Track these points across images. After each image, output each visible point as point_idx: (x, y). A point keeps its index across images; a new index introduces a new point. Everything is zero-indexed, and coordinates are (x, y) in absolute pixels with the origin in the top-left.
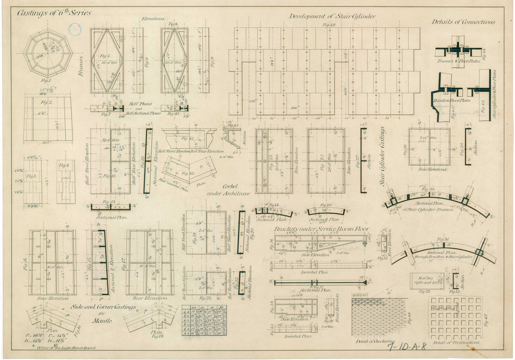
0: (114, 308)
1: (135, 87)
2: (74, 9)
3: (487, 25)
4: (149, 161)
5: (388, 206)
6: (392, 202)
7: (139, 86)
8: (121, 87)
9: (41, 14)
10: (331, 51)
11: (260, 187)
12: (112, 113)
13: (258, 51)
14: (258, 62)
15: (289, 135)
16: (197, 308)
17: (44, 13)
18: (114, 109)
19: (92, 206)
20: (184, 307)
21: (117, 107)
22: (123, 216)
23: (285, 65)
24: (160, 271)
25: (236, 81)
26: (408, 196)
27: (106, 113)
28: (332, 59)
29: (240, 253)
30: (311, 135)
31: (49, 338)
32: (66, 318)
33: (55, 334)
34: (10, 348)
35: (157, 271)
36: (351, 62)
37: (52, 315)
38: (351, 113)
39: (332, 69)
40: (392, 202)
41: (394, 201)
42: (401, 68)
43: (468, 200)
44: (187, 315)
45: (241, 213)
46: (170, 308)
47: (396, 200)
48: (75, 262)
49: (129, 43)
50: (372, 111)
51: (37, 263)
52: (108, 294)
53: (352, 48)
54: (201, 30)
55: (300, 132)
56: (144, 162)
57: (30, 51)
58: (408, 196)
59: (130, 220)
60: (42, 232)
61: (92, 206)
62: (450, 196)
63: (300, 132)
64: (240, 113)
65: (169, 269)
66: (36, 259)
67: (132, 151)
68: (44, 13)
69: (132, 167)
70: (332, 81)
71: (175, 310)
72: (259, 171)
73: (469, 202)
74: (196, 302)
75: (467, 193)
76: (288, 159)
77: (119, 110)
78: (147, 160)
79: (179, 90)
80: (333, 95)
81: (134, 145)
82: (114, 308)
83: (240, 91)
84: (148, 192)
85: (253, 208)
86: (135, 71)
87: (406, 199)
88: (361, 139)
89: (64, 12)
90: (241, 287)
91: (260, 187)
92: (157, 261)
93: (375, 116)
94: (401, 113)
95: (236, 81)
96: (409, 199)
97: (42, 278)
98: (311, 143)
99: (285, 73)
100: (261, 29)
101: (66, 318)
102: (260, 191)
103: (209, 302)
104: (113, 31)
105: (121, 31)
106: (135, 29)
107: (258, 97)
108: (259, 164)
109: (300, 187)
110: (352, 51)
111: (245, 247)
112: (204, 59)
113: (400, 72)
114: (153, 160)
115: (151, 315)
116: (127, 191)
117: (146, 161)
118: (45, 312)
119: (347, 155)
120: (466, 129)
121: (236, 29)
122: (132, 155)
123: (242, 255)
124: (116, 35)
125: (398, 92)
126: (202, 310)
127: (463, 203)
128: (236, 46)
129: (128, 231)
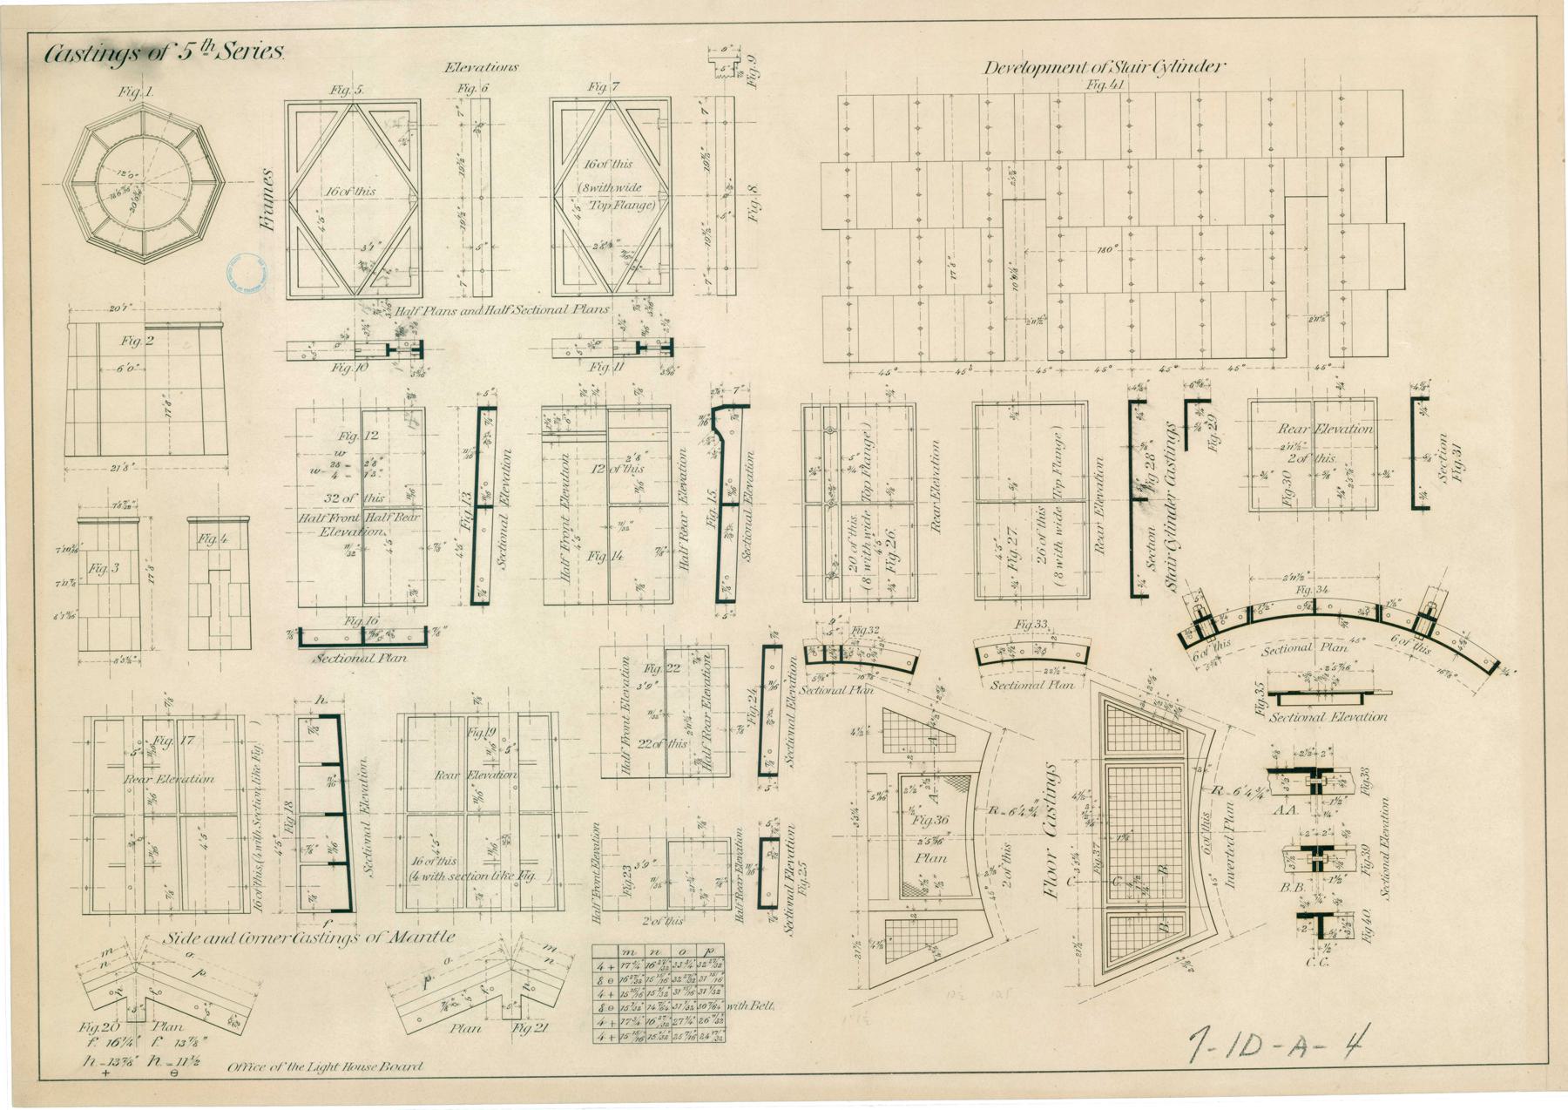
1: (467, 278)
2: (233, 36)
4: (486, 507)
6: (1198, 630)
7: (722, 273)
8: (666, 277)
10: (992, 165)
11: (815, 583)
12: (631, 363)
13: (1052, 166)
14: (1335, 197)
16: (640, 952)
20: (598, 952)
21: (651, 342)
23: (852, 209)
24: (515, 840)
25: (986, 257)
26: (1250, 610)
28: (1278, 186)
30: (982, 424)
32: (193, 981)
33: (171, 1037)
34: (34, 1076)
35: (506, 840)
37: (158, 976)
38: (1337, 352)
39: (1279, 219)
40: (1198, 630)
41: (1207, 628)
42: (852, 217)
43: (1434, 620)
44: (606, 977)
46: (551, 956)
47: (1213, 623)
49: (690, 139)
52: (350, 911)
54: (708, 106)
56: (472, 510)
57: (86, 172)
65: (549, 832)
66: (110, 800)
67: (677, 473)
69: (677, 522)
71: (568, 961)
72: (814, 536)
74: (627, 931)
75: (1430, 598)
78: (480, 502)
79: (374, 291)
83: (1280, 286)
89: (195, 49)
91: (815, 583)
92: (505, 809)
93: (1269, 363)
95: (986, 257)
97: (130, 861)
100: (1132, 97)
101: (193, 981)
102: (818, 595)
103: (674, 934)
106: (711, 100)
107: (1055, 308)
108: (814, 514)
113: (851, 233)
114: (497, 503)
115: (481, 978)
116: (663, 594)
117: (722, 505)
118: (140, 969)
119: (1094, 482)
120: (1187, 402)
121: (842, 100)
122: (677, 487)
126: (661, 963)
127: (1418, 629)
128: (984, 150)
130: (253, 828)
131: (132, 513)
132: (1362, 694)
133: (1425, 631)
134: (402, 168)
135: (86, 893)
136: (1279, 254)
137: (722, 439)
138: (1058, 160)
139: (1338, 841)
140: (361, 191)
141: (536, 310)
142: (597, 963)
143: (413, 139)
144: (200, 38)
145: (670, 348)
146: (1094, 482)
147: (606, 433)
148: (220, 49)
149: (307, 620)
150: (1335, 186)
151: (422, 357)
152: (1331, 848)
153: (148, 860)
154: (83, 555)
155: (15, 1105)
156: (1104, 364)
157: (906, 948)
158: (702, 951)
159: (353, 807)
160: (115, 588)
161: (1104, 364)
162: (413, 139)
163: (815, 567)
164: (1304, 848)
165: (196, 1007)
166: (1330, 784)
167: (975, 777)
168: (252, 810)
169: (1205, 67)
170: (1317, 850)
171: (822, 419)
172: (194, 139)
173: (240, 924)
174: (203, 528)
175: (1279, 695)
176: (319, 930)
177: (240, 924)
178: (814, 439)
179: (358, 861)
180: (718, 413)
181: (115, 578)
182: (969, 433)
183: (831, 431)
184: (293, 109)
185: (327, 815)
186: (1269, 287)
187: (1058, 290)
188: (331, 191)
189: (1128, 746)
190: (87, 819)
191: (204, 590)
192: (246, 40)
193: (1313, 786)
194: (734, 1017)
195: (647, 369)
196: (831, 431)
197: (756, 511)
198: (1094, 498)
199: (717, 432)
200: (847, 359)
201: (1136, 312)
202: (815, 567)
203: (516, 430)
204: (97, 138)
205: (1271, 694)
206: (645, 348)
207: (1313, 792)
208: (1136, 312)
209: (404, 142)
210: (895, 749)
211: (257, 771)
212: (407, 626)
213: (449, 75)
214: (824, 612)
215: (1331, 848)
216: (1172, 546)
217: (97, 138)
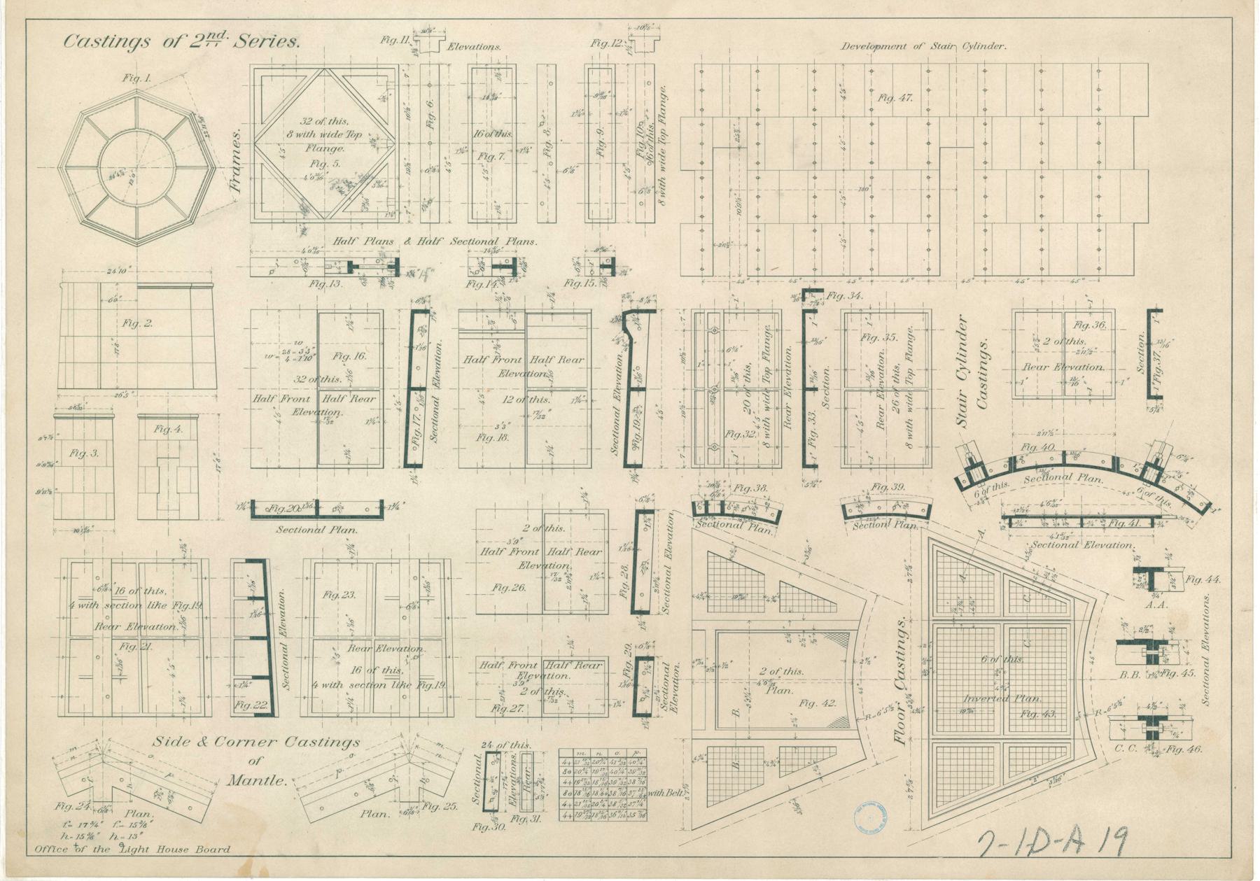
3: (894, 51)
9: (134, 44)
17: (142, 42)
18: (351, 267)
19: (253, 507)
27: (321, 280)
29: (642, 613)
31: (64, 830)
36: (753, 149)
39: (935, 165)
43: (981, 464)
45: (258, 512)
47: (1159, 476)
61: (253, 507)
62: (1116, 461)
64: (934, 271)
70: (708, 195)
73: (988, 468)
80: (935, 228)
86: (444, 173)
96: (1016, 470)
99: (875, 174)
100: (817, 67)
110: (756, 121)
121: (698, 68)
123: (644, 617)
132: (1152, 518)
135: (208, 692)
136: (934, 195)
137: (631, 338)
139: (1173, 711)
147: (525, 331)
152: (1165, 718)
153: (116, 673)
155: (7, 876)
157: (742, 787)
159: (275, 632)
162: (391, 99)
164: (1141, 718)
165: (356, 794)
166: (1170, 654)
167: (853, 634)
169: (993, 46)
170: (1153, 720)
179: (279, 677)
180: (628, 317)
183: (715, 331)
184: (259, 73)
185: (253, 638)
186: (925, 219)
189: (1046, 609)
193: (1149, 657)
200: (700, 273)
204: (136, 105)
206: (357, 267)
210: (717, 609)
214: (709, 476)
215: (1165, 718)
217: (136, 105)
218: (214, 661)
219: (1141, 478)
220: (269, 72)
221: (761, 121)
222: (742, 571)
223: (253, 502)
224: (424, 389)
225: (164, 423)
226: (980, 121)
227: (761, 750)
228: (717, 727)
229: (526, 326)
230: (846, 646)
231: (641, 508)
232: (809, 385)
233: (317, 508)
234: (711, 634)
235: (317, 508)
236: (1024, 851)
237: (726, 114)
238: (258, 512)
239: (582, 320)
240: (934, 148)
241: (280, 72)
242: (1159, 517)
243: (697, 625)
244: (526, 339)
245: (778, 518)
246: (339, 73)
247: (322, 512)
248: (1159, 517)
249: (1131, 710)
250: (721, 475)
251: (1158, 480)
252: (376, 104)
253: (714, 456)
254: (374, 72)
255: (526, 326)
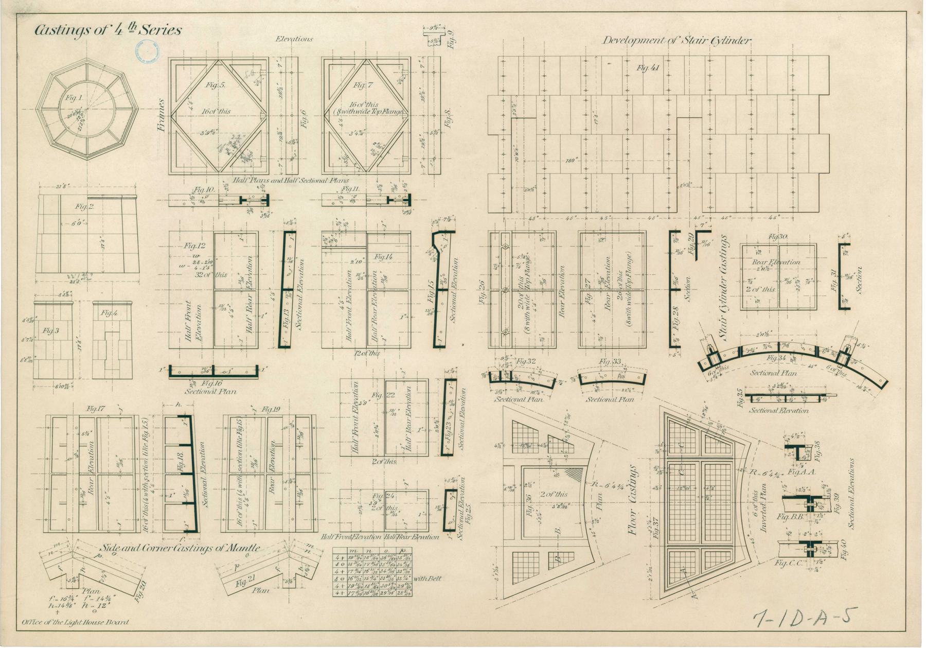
0: (172, 549)
4: (443, 290)
5: (704, 367)
11: (496, 336)
14: (540, 119)
15: (548, 242)
17: (85, 31)
18: (389, 200)
22: (628, 395)
26: (740, 349)
28: (673, 112)
39: (673, 131)
40: (839, 355)
43: (717, 352)
45: (173, 373)
47: (848, 360)
48: (315, 471)
50: (744, 206)
51: (61, 474)
53: (708, 92)
54: (282, 63)
55: (567, 240)
58: (740, 349)
59: (244, 396)
60: (286, 418)
62: (817, 349)
63: (567, 240)
64: (673, 209)
66: (59, 466)
68: (85, 31)
73: (721, 355)
75: (705, 344)
76: (547, 286)
77: (400, 203)
81: (302, 264)
82: (172, 549)
83: (673, 170)
84: (288, 345)
85: (486, 371)
87: (736, 355)
88: (670, 253)
90: (449, 513)
91: (496, 336)
94: (795, 210)
96: (743, 356)
97: (286, 502)
98: (584, 258)
104: (380, 62)
105: (405, 62)
106: (284, 59)
107: (541, 182)
109: (567, 339)
111: (457, 441)
112: (289, 113)
124: (389, 71)
125: (625, 171)
129: (226, 417)
130: (143, 482)
131: (69, 298)
132: (819, 395)
133: (718, 361)
134: (257, 100)
138: (544, 95)
140: (221, 111)
141: (312, 181)
142: (335, 556)
143: (264, 82)
144: (127, 20)
145: (409, 200)
146: (559, 279)
147: (366, 247)
148: (140, 28)
149: (173, 358)
150: (540, 113)
151: (268, 205)
154: (36, 322)
156: (653, 214)
158: (399, 550)
160: (57, 344)
161: (653, 214)
162: (264, 82)
163: (496, 328)
164: (801, 542)
168: (143, 471)
170: (810, 544)
171: (500, 243)
172: (119, 82)
173: (135, 540)
174: (102, 308)
175: (751, 395)
176: (176, 542)
177: (135, 540)
178: (496, 252)
181: (57, 336)
182: (576, 250)
183: (506, 247)
187: (709, 171)
188: (205, 111)
190: (225, 476)
191: (103, 343)
192: (157, 21)
194: (418, 587)
195: (395, 214)
196: (506, 247)
197: (458, 293)
198: (559, 288)
199: (435, 247)
200: (584, 210)
201: (795, 184)
202: (496, 328)
203: (306, 248)
204: (58, 81)
205: (747, 395)
206: (245, 200)
207: (808, 511)
208: (795, 184)
209: (258, 83)
211: (145, 448)
212: (241, 363)
213: (278, 43)
214: (501, 353)
216: (723, 309)
217: (58, 81)
218: (41, 486)
219: (836, 362)
220: (182, 62)
221: (712, 98)
222: (526, 430)
223: (170, 366)
224: (292, 290)
225: (109, 308)
226: (541, 98)
227: (536, 555)
228: (523, 535)
229: (367, 243)
230: (580, 481)
231: (448, 377)
232: (673, 287)
233: (213, 370)
234: (518, 469)
235: (213, 370)
236: (786, 626)
237: (687, 93)
238: (173, 373)
239: (404, 239)
240: (673, 118)
241: (189, 62)
242: (824, 395)
243: (507, 462)
244: (367, 253)
245: (185, 416)
246: (228, 63)
247: (216, 373)
248: (824, 395)
249: (795, 538)
250: (510, 352)
251: (847, 363)
252: (395, 84)
253: (506, 341)
254: (251, 62)
255: (367, 243)
